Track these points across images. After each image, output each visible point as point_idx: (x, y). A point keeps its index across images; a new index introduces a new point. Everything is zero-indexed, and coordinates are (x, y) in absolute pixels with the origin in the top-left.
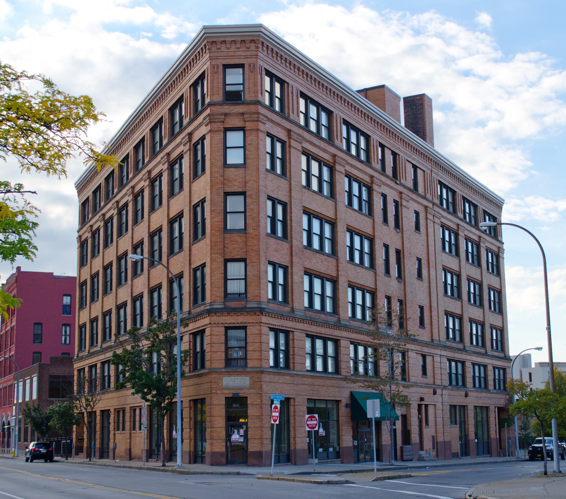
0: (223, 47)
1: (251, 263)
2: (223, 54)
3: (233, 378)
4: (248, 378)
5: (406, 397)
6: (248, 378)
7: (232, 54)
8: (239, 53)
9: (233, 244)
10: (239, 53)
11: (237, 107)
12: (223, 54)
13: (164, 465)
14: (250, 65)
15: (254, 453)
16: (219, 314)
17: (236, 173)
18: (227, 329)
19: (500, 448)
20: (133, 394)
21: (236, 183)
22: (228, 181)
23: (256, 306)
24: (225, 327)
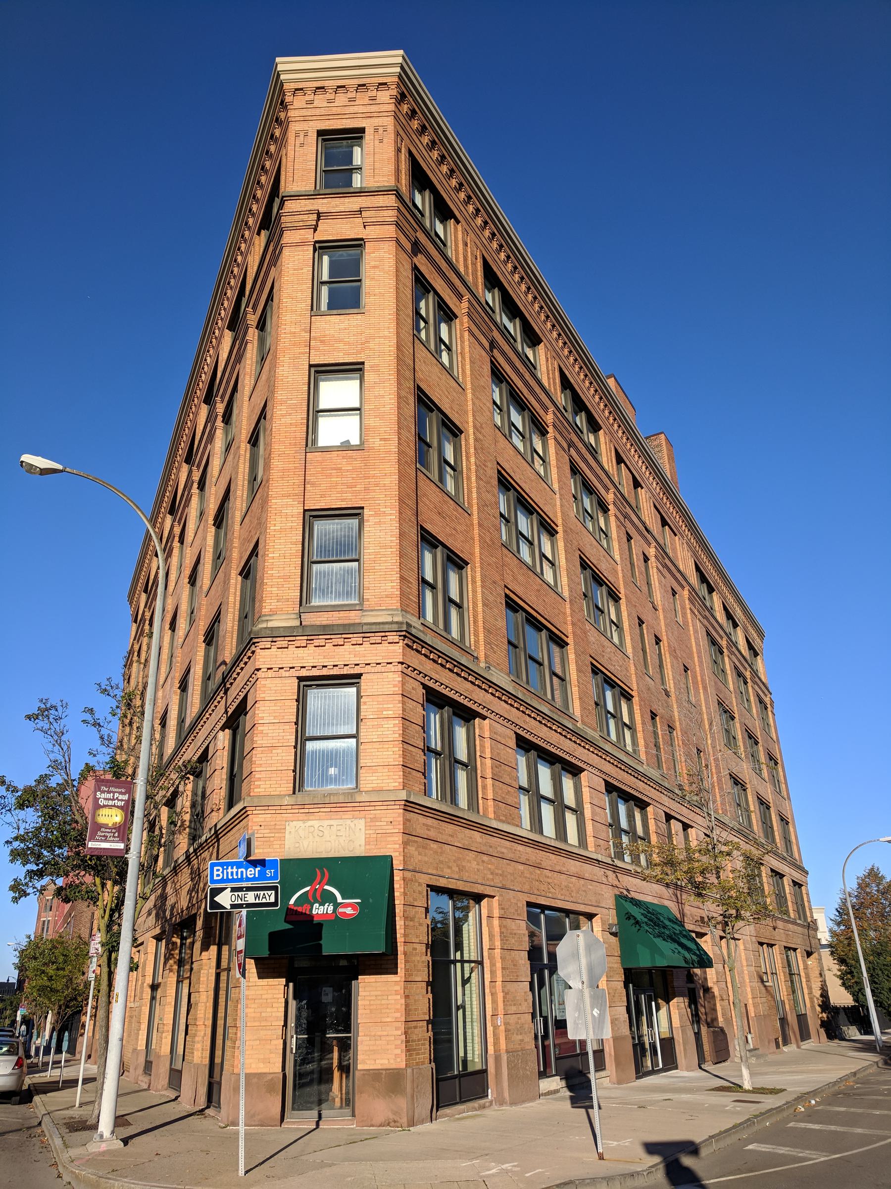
0: (320, 100)
1: (377, 514)
2: (318, 112)
3: (316, 823)
4: (361, 824)
5: (705, 962)
6: (361, 824)
7: (339, 110)
8: (352, 109)
9: (330, 476)
10: (352, 109)
11: (347, 200)
12: (318, 112)
13: (323, 283)
14: (376, 130)
15: (375, 1075)
16: (284, 644)
17: (342, 326)
18: (307, 682)
19: (20, 1130)
20: (29, 937)
21: (341, 346)
22: (322, 342)
23: (389, 619)
24: (298, 678)
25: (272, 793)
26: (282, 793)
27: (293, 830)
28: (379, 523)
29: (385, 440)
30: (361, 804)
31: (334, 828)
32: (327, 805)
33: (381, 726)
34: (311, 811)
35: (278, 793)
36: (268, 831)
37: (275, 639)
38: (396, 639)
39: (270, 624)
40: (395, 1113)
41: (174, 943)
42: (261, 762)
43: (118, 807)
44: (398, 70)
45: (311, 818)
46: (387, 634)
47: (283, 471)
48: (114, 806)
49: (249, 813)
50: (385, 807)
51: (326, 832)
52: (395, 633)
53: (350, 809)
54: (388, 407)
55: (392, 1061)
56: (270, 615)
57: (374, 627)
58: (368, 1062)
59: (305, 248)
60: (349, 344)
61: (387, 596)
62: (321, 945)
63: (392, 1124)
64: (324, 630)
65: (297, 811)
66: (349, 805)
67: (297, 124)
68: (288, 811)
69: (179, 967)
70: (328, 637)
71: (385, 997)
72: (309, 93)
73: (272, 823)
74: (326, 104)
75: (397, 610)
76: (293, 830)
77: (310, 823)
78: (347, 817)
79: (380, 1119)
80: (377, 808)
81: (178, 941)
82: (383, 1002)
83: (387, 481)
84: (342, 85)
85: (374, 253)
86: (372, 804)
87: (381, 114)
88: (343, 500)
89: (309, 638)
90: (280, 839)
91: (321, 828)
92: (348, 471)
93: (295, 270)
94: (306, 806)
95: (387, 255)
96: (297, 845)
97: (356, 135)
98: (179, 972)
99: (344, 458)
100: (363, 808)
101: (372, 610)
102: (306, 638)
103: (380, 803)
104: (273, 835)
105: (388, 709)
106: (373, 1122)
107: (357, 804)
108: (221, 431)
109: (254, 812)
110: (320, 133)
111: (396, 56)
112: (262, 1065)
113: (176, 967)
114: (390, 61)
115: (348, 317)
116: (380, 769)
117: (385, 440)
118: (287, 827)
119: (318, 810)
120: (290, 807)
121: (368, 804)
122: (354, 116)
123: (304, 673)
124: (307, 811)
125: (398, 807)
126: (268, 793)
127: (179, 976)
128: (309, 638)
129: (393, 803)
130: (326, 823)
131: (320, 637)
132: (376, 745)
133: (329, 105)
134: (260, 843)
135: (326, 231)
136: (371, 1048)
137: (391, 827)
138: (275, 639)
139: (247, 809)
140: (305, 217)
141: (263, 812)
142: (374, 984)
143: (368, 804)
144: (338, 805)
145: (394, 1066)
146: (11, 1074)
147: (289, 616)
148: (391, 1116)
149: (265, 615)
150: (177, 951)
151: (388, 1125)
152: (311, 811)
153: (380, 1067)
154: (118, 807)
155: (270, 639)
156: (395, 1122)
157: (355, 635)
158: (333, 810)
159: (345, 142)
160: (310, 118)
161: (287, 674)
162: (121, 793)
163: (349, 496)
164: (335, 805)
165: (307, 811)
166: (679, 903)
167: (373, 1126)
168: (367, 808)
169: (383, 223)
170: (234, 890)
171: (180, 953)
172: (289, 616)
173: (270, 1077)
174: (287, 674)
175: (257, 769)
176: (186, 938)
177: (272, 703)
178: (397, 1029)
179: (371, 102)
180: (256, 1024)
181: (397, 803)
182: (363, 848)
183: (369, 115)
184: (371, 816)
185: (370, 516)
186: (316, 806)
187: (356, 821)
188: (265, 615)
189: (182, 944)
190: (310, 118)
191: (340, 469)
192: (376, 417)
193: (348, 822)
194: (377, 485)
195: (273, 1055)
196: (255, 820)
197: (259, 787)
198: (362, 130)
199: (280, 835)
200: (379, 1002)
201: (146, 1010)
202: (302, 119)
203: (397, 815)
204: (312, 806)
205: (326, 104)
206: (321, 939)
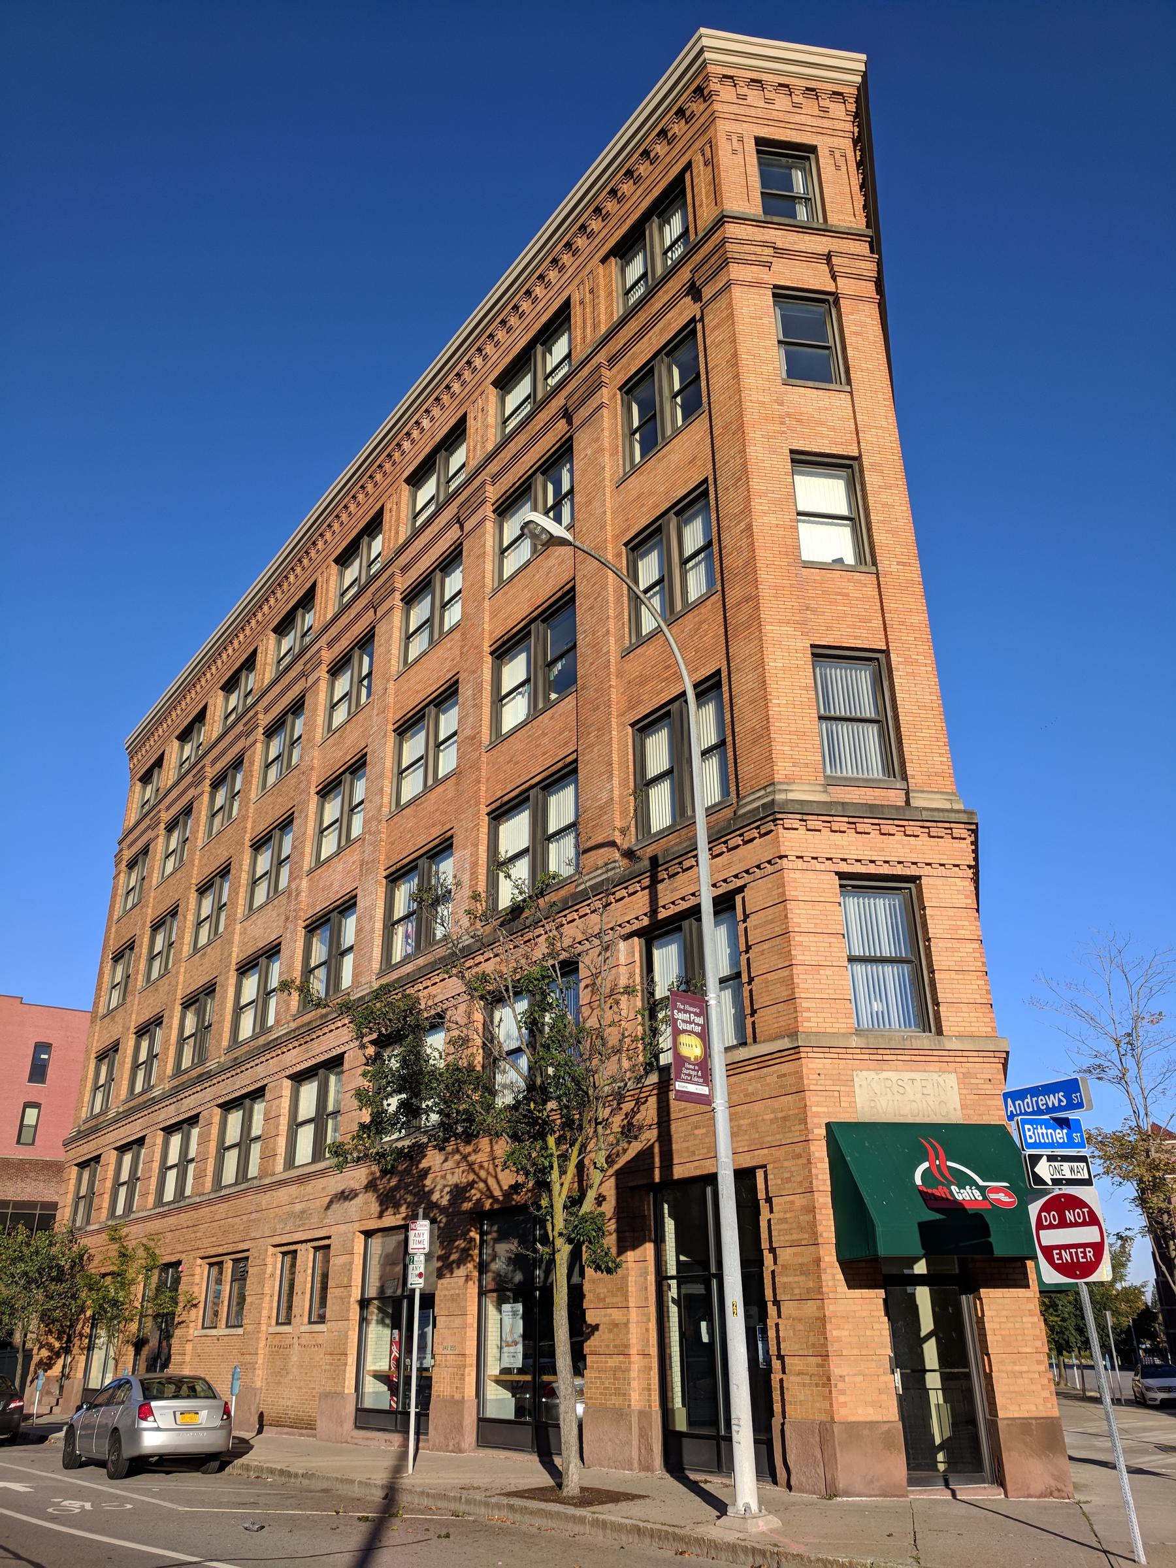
0: (782, 102)
4: (951, 1080)
6: (951, 1080)
9: (835, 603)
11: (807, 237)
16: (818, 824)
21: (825, 430)
23: (948, 806)
25: (828, 1030)
26: (842, 1031)
27: (864, 1083)
28: (913, 674)
29: (904, 564)
30: (951, 1053)
31: (918, 1083)
32: (906, 1052)
33: (957, 950)
34: (885, 1058)
35: (835, 1030)
36: (830, 1082)
37: (805, 817)
38: (965, 833)
39: (791, 796)
40: (1056, 1479)
41: (472, 1240)
42: (806, 986)
43: (695, 1033)
44: (859, 79)
45: (885, 1067)
46: (952, 825)
47: (776, 587)
48: (692, 1032)
49: (802, 1055)
50: (981, 1060)
51: (908, 1089)
52: (962, 826)
53: (936, 1059)
54: (901, 522)
55: (1041, 1408)
56: (787, 784)
57: (936, 814)
58: (1011, 1408)
59: (762, 291)
60: (833, 429)
61: (937, 774)
62: (991, 1244)
63: (1056, 1494)
64: (872, 812)
65: (866, 1057)
66: (935, 1053)
67: (727, 122)
68: (855, 1056)
69: (481, 1273)
70: (876, 821)
71: (1019, 1319)
72: (742, 84)
73: (835, 1072)
74: (762, 104)
75: (952, 794)
76: (864, 1083)
77: (885, 1074)
78: (931, 1069)
79: (1038, 1486)
80: (970, 1059)
81: (477, 1237)
82: (1017, 1326)
83: (915, 619)
84: (778, 86)
85: (852, 314)
86: (965, 1054)
87: (836, 133)
88: (856, 637)
89: (851, 820)
90: (848, 1094)
91: (900, 1083)
92: (857, 599)
93: (751, 318)
94: (880, 1051)
95: (868, 320)
96: (873, 1104)
97: (804, 153)
98: (480, 1281)
99: (849, 581)
100: (952, 1059)
101: (922, 792)
102: (846, 819)
103: (976, 1054)
104: (838, 1088)
105: (963, 927)
106: (1032, 1492)
107: (946, 1053)
108: (491, 524)
109: (810, 1055)
110: (760, 141)
111: (856, 61)
112: (871, 1410)
113: (476, 1274)
114: (849, 65)
115: (827, 393)
116: (964, 1008)
117: (904, 564)
118: (856, 1079)
119: (894, 1057)
120: (858, 1051)
121: (960, 1053)
122: (800, 127)
123: (844, 868)
124: (880, 1057)
125: (997, 1060)
126: (823, 1030)
127: (480, 1287)
128: (851, 820)
129: (992, 1054)
130: (906, 1076)
131: (866, 820)
132: (953, 975)
133: (767, 106)
134: (817, 1099)
135: (783, 273)
136: (1012, 1388)
137: (990, 1087)
138: (805, 817)
139: (802, 1049)
140: (758, 250)
141: (821, 1055)
142: (1000, 1301)
143: (960, 1053)
144: (921, 1052)
145: (1043, 1415)
146: (221, 1427)
147: (813, 788)
148: (1053, 1483)
149: (781, 783)
150: (477, 1251)
151: (1051, 1494)
152: (885, 1058)
153: (1026, 1415)
154: (695, 1033)
155: (799, 817)
156: (1059, 1490)
157: (911, 823)
158: (914, 1058)
159: (784, 160)
160: (744, 118)
161: (823, 867)
162: (696, 1014)
163: (863, 633)
164: (917, 1052)
165: (880, 1057)
166: (99, 1231)
167: (1030, 1496)
168: (958, 1059)
169: (859, 277)
170: (1051, 1158)
171: (481, 1254)
172: (813, 788)
173: (885, 1427)
174: (823, 867)
175: (803, 995)
176: (487, 1233)
177: (809, 906)
178: (1039, 1362)
179: (822, 114)
180: (855, 1352)
181: (997, 1054)
182: (959, 1112)
183: (819, 130)
184: (964, 1070)
185: (899, 663)
186: (892, 1052)
187: (945, 1076)
188: (781, 783)
189: (482, 1242)
190: (744, 118)
191: (847, 595)
192: (887, 532)
193: (935, 1076)
194: (902, 623)
195: (884, 1397)
196: (810, 1066)
197: (808, 1020)
198: (813, 149)
199: (847, 1089)
200: (1011, 1326)
201: (354, 1336)
202: (733, 117)
203: (995, 1071)
204: (888, 1052)
205: (762, 104)
206: (989, 1235)
